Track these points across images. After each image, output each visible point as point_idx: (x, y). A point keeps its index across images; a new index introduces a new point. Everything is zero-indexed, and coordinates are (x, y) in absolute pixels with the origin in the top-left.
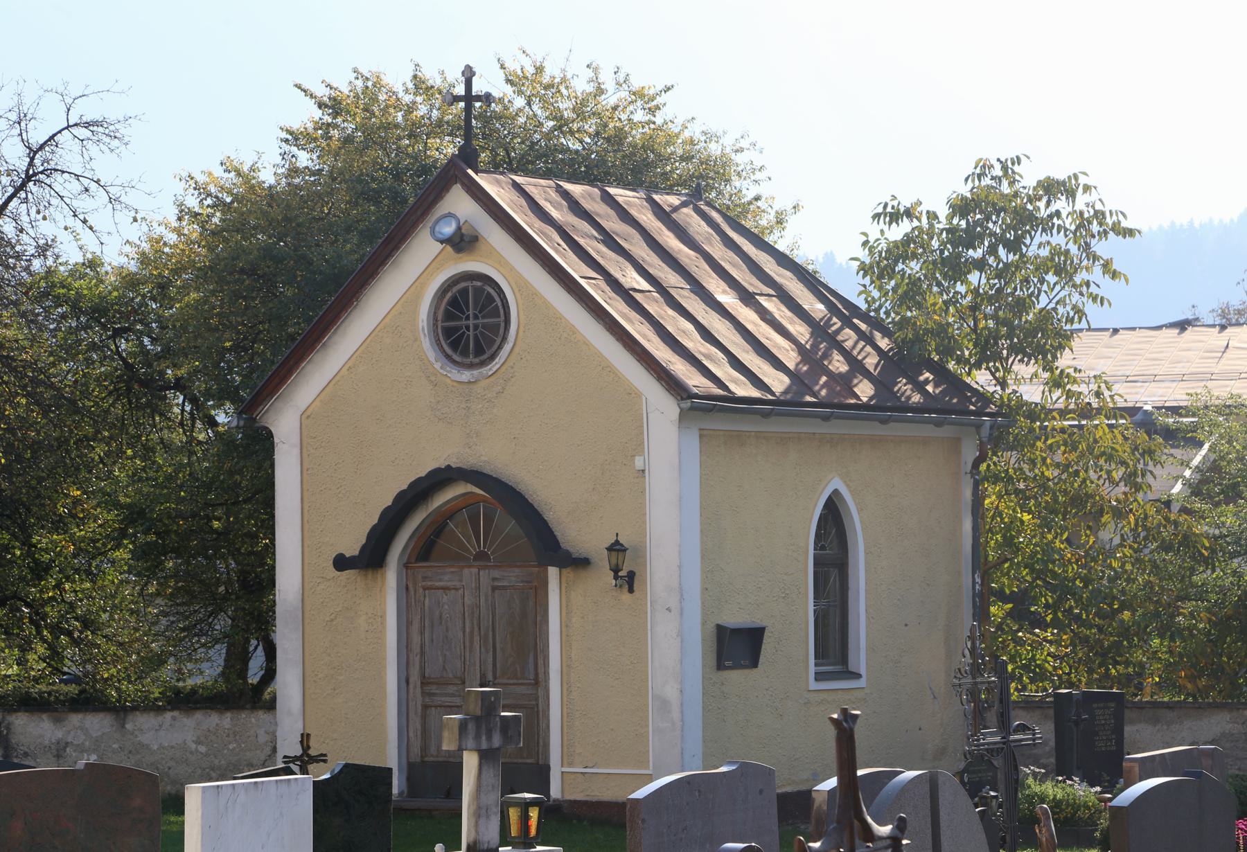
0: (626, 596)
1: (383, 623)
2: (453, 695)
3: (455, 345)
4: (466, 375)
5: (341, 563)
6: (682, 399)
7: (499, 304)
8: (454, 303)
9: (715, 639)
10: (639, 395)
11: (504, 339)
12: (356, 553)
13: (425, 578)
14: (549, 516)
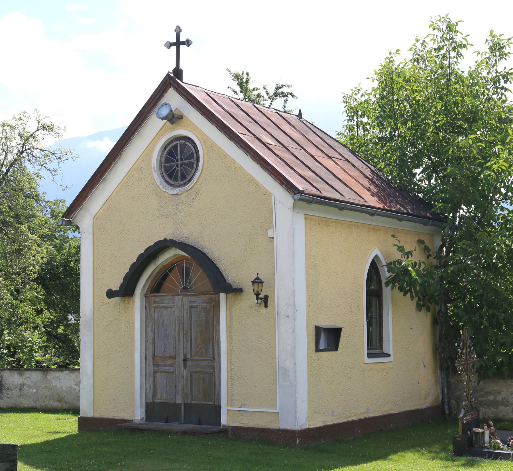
0: (263, 310)
1: (133, 327)
2: (169, 366)
3: (170, 176)
4: (176, 191)
5: (110, 294)
6: (295, 194)
7: (194, 151)
8: (170, 153)
9: (314, 334)
10: (270, 195)
11: (196, 170)
12: (118, 289)
13: (155, 302)
14: (220, 266)
